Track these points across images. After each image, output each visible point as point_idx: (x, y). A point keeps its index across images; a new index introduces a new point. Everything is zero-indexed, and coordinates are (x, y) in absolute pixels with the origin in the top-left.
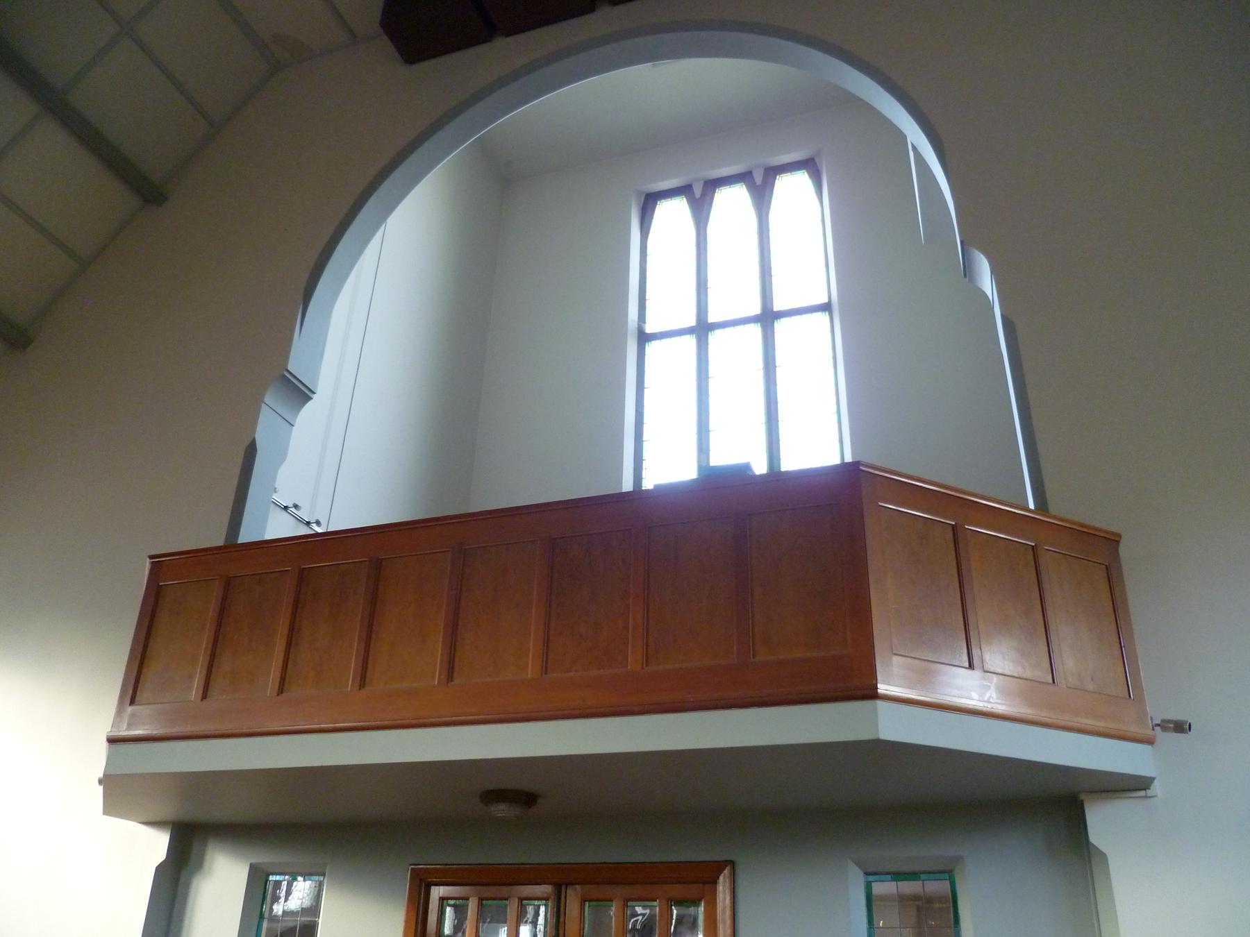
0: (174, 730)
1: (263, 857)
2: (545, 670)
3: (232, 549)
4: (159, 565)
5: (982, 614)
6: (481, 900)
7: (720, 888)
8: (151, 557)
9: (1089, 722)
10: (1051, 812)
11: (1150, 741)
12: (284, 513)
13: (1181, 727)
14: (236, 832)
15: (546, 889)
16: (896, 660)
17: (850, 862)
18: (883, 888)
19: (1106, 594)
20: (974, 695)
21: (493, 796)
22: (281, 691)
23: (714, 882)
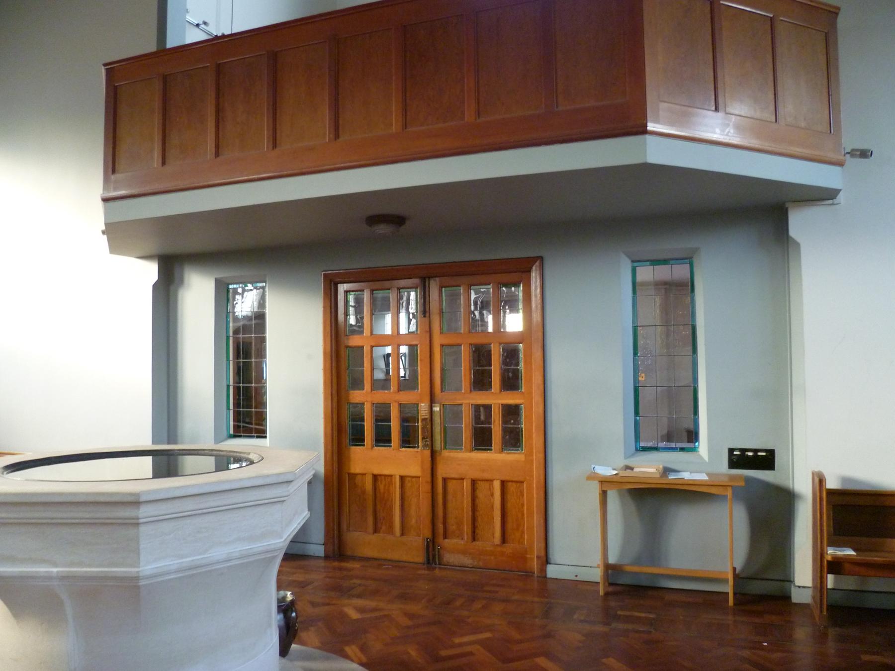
0: (148, 189)
1: (224, 273)
2: (405, 126)
3: (164, 54)
4: (113, 71)
5: (728, 75)
6: (372, 291)
7: (533, 274)
8: (105, 65)
9: (798, 150)
10: (763, 215)
11: (840, 164)
12: (196, 29)
13: (865, 154)
14: (203, 258)
15: (416, 281)
16: (663, 106)
17: (623, 256)
18: (646, 273)
19: (823, 58)
20: (718, 130)
21: (374, 220)
22: (217, 154)
23: (529, 271)
